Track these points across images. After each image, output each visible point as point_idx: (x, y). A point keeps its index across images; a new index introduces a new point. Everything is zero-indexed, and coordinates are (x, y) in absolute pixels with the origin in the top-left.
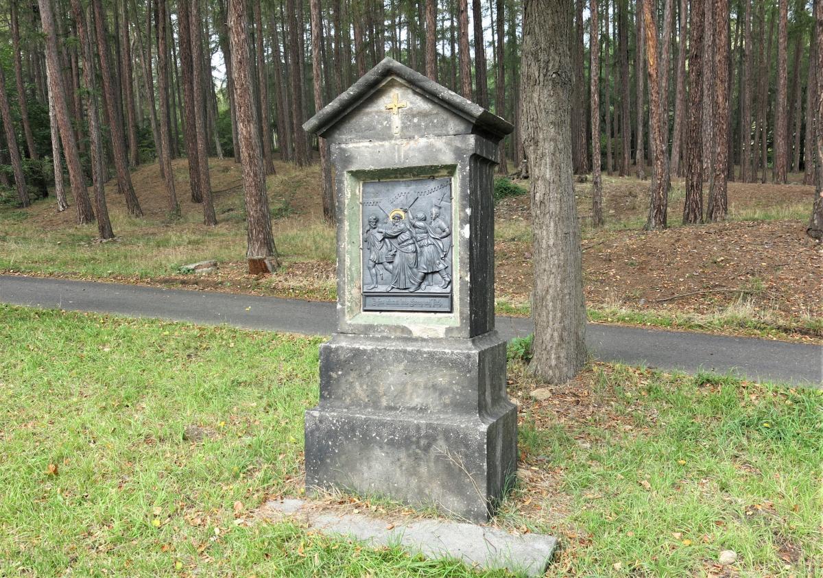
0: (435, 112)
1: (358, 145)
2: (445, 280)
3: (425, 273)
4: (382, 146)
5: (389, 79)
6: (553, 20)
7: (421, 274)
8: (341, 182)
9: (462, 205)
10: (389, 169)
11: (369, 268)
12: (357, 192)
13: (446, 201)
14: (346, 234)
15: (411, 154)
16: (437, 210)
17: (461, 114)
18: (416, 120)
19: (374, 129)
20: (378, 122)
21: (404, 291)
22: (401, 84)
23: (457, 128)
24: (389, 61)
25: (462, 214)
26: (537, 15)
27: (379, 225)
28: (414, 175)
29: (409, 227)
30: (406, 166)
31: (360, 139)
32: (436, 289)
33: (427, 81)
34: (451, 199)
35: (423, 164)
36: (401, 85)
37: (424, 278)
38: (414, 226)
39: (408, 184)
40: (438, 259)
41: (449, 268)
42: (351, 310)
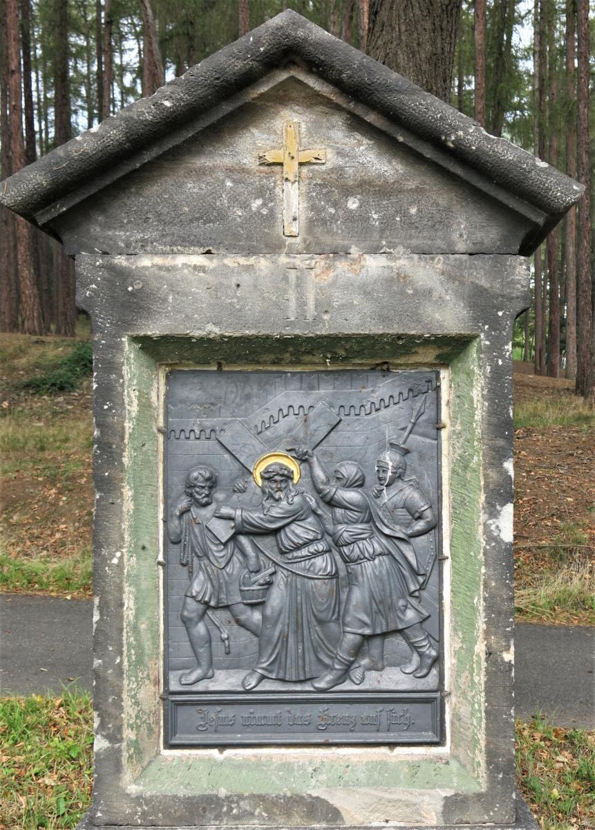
0: (412, 184)
1: (168, 261)
2: (421, 655)
3: (363, 636)
4: (249, 268)
5: (283, 76)
6: (434, 43)
7: (350, 639)
8: (112, 367)
9: (493, 449)
10: (268, 337)
11: (186, 622)
12: (153, 395)
13: (424, 435)
14: (125, 525)
15: (338, 298)
16: (398, 457)
17: (503, 197)
18: (353, 204)
19: (222, 216)
20: (234, 199)
21: (298, 688)
22: (317, 95)
23: (479, 235)
24: (295, 24)
25: (493, 475)
26: (403, 28)
27: (220, 496)
28: (334, 360)
29: (313, 503)
30: (323, 331)
31: (173, 244)
32: (395, 679)
33: (414, 92)
34: (439, 429)
35: (378, 329)
36: (313, 100)
37: (358, 651)
38: (331, 503)
39: (309, 382)
40: (403, 597)
41: (431, 625)
42: (138, 750)
